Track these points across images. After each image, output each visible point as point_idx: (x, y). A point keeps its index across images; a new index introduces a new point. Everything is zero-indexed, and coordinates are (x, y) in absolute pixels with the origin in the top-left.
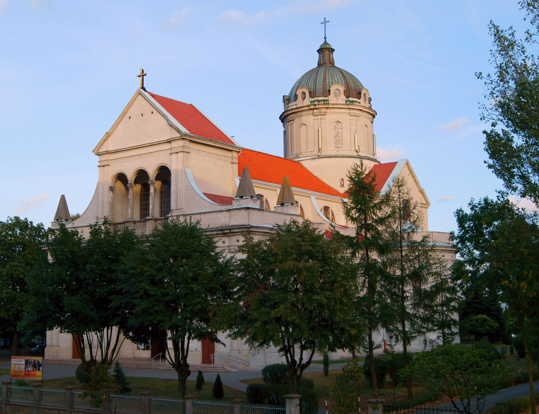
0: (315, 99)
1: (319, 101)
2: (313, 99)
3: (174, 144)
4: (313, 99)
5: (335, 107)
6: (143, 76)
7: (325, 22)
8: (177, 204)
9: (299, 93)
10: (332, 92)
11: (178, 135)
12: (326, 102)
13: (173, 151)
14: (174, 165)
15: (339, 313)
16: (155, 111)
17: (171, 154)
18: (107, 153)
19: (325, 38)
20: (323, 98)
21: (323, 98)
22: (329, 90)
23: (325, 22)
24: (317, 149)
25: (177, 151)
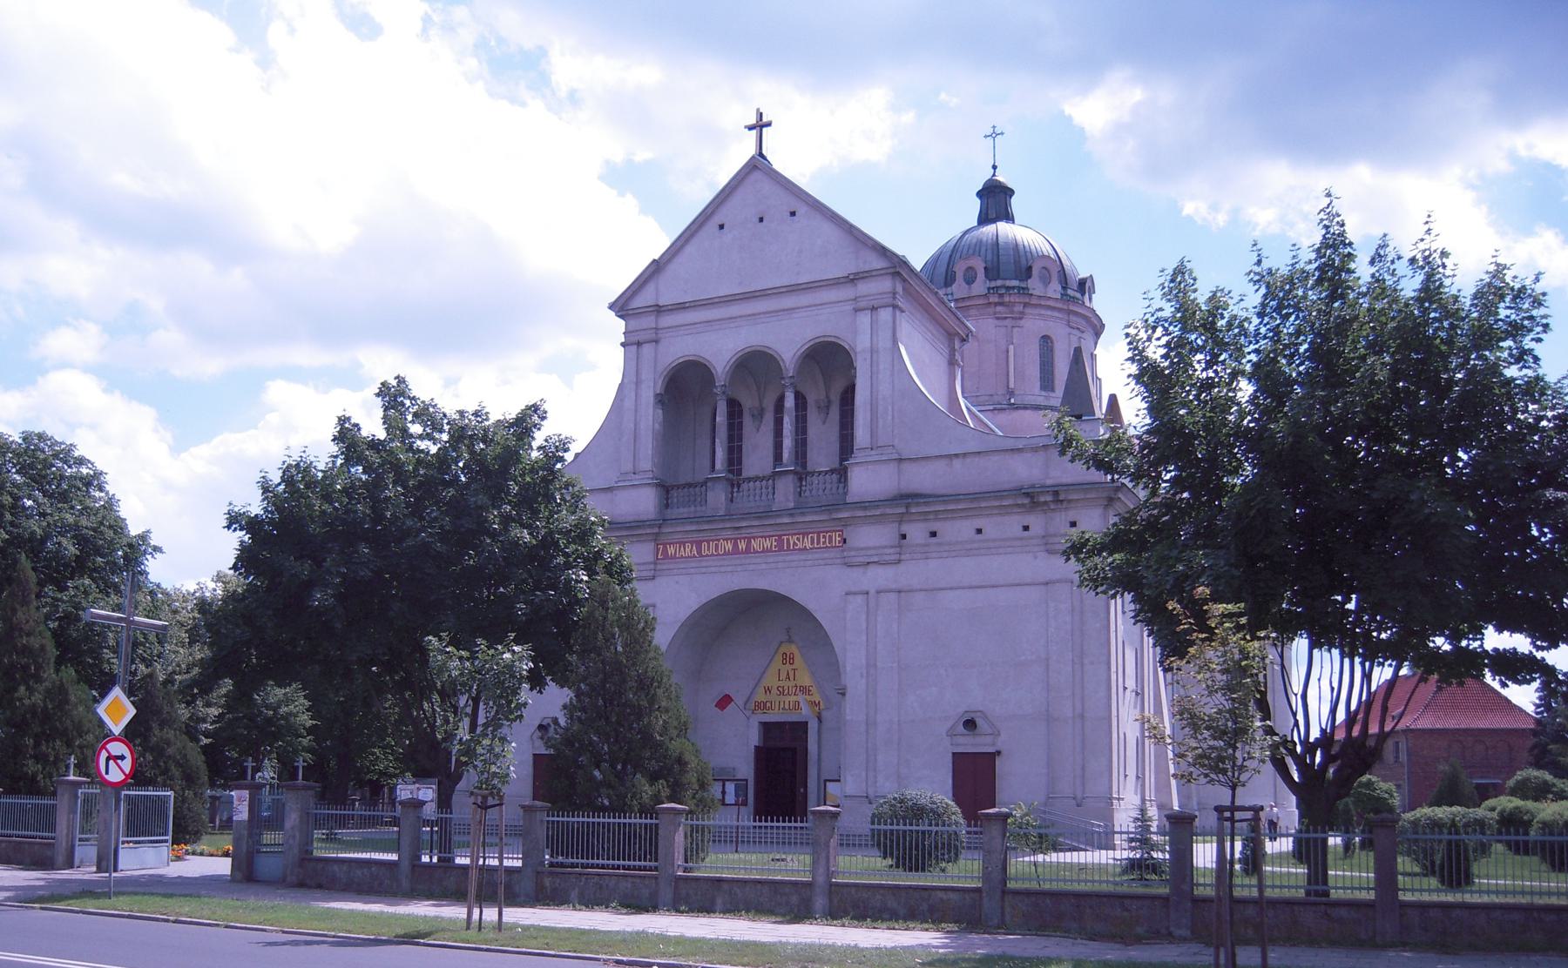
0: (999, 283)
1: (1008, 288)
2: (993, 284)
3: (863, 288)
4: (993, 284)
5: (1042, 304)
6: (762, 127)
7: (994, 135)
8: (873, 434)
9: (960, 269)
10: (1035, 272)
11: (878, 263)
12: (1023, 291)
13: (862, 304)
14: (860, 337)
15: (436, 697)
16: (802, 210)
17: (856, 310)
18: (659, 310)
19: (995, 167)
20: (1015, 283)
21: (1015, 283)
22: (1030, 268)
23: (994, 135)
24: (1002, 391)
25: (876, 303)
